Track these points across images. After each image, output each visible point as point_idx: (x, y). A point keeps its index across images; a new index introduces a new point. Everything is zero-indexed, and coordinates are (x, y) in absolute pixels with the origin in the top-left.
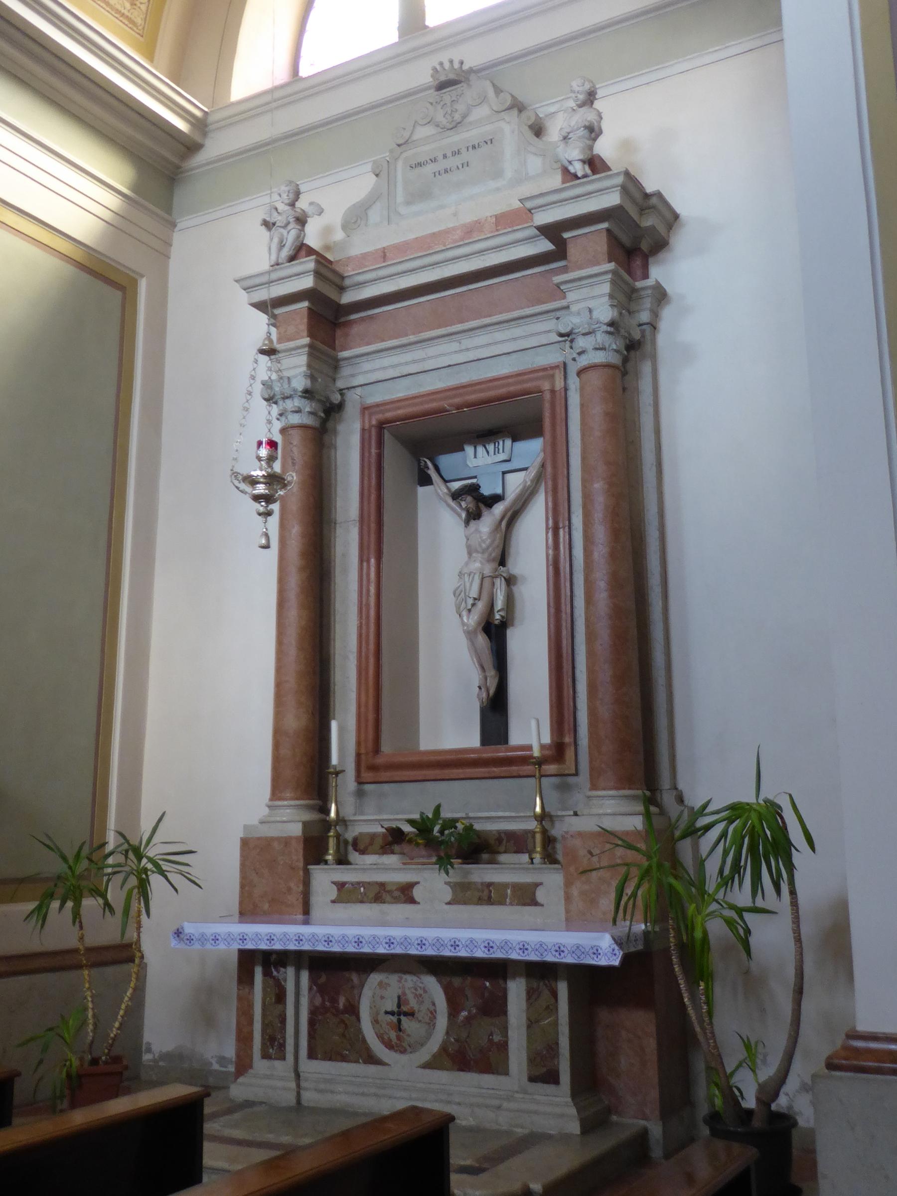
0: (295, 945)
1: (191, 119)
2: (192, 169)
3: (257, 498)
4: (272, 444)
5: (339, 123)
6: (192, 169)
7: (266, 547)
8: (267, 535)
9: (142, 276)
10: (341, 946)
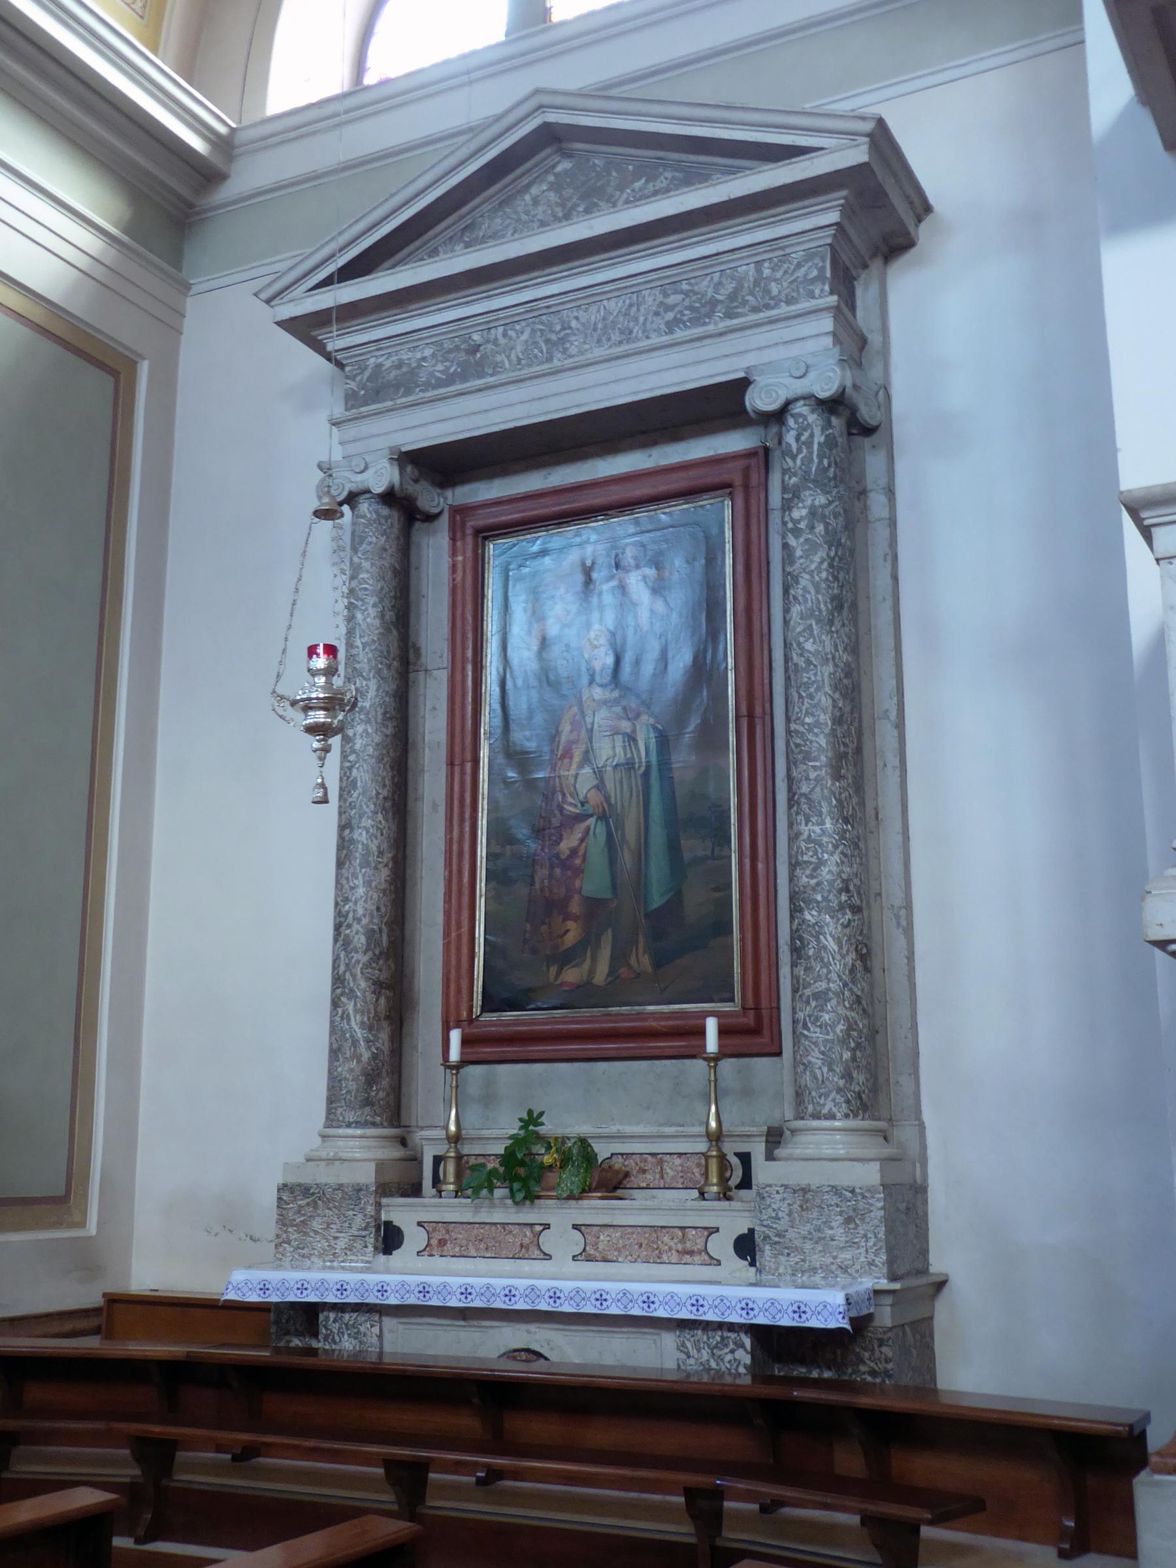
1: (209, 135)
2: (216, 208)
3: (312, 729)
4: (331, 650)
6: (216, 208)
7: (324, 800)
8: (323, 786)
9: (144, 359)
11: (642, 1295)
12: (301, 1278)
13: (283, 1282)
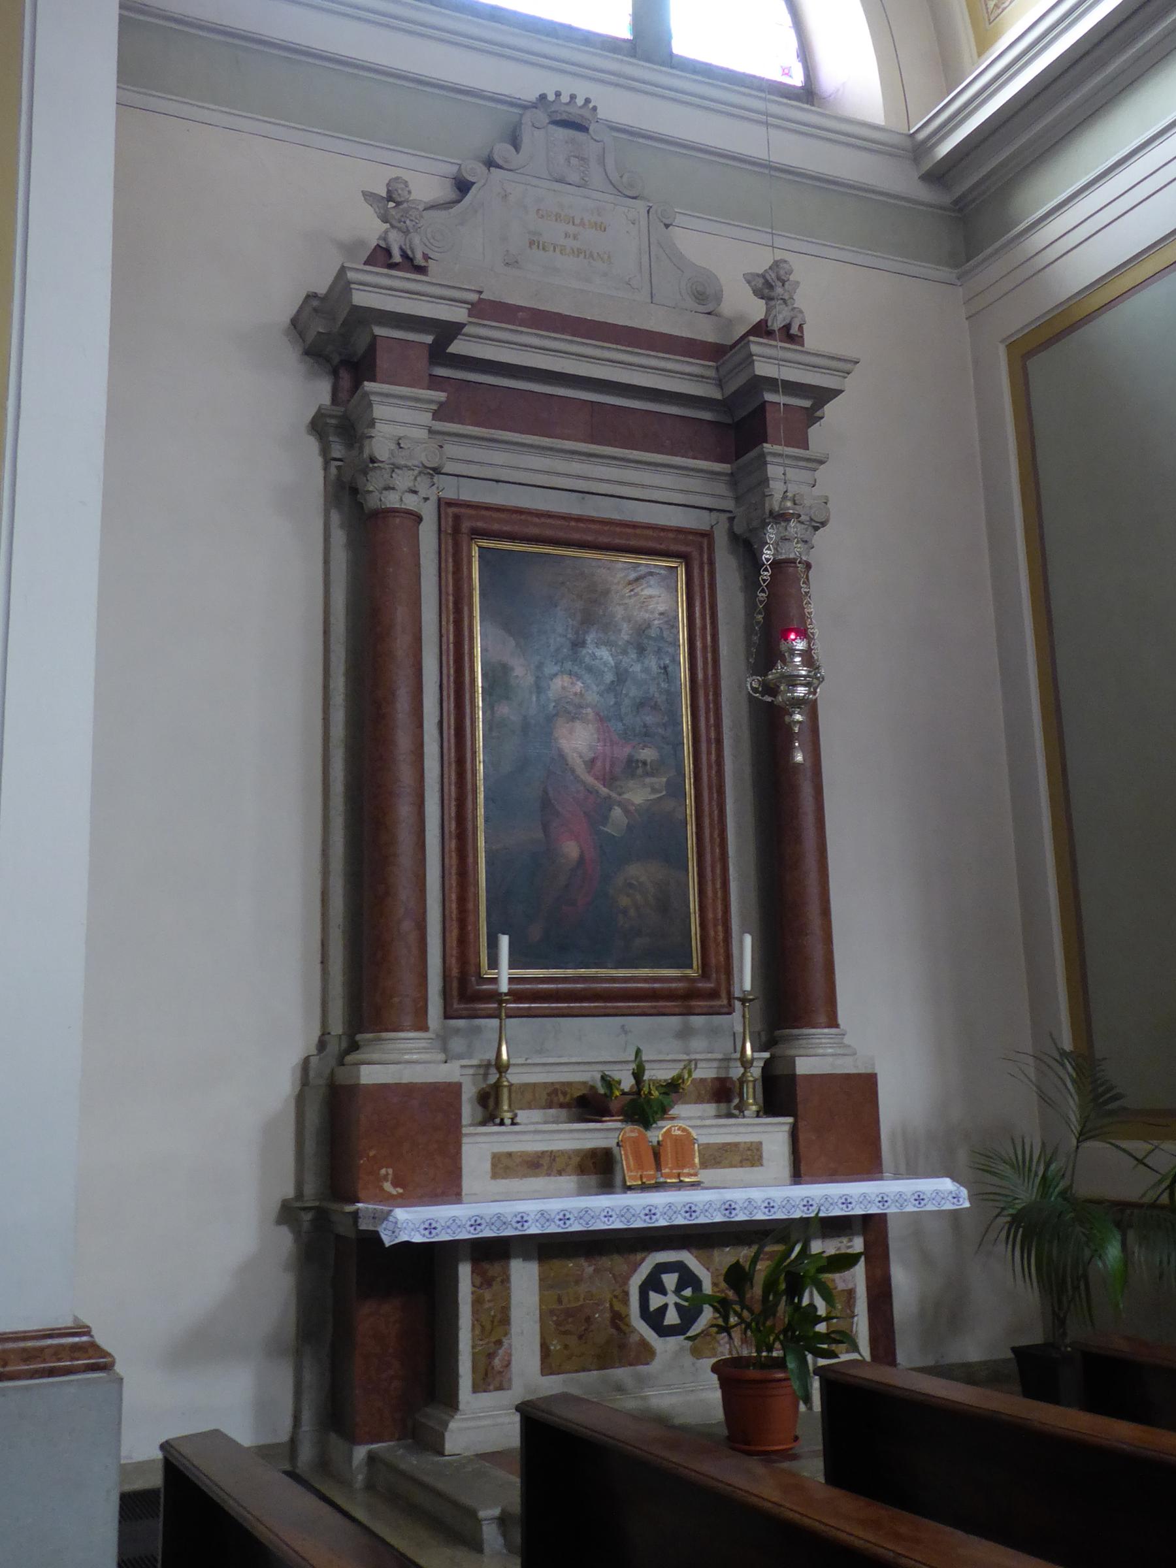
0: (645, 1221)
5: (331, 65)
10: (540, 1226)
11: (803, 1200)
12: (473, 1214)
13: (670, 1205)
